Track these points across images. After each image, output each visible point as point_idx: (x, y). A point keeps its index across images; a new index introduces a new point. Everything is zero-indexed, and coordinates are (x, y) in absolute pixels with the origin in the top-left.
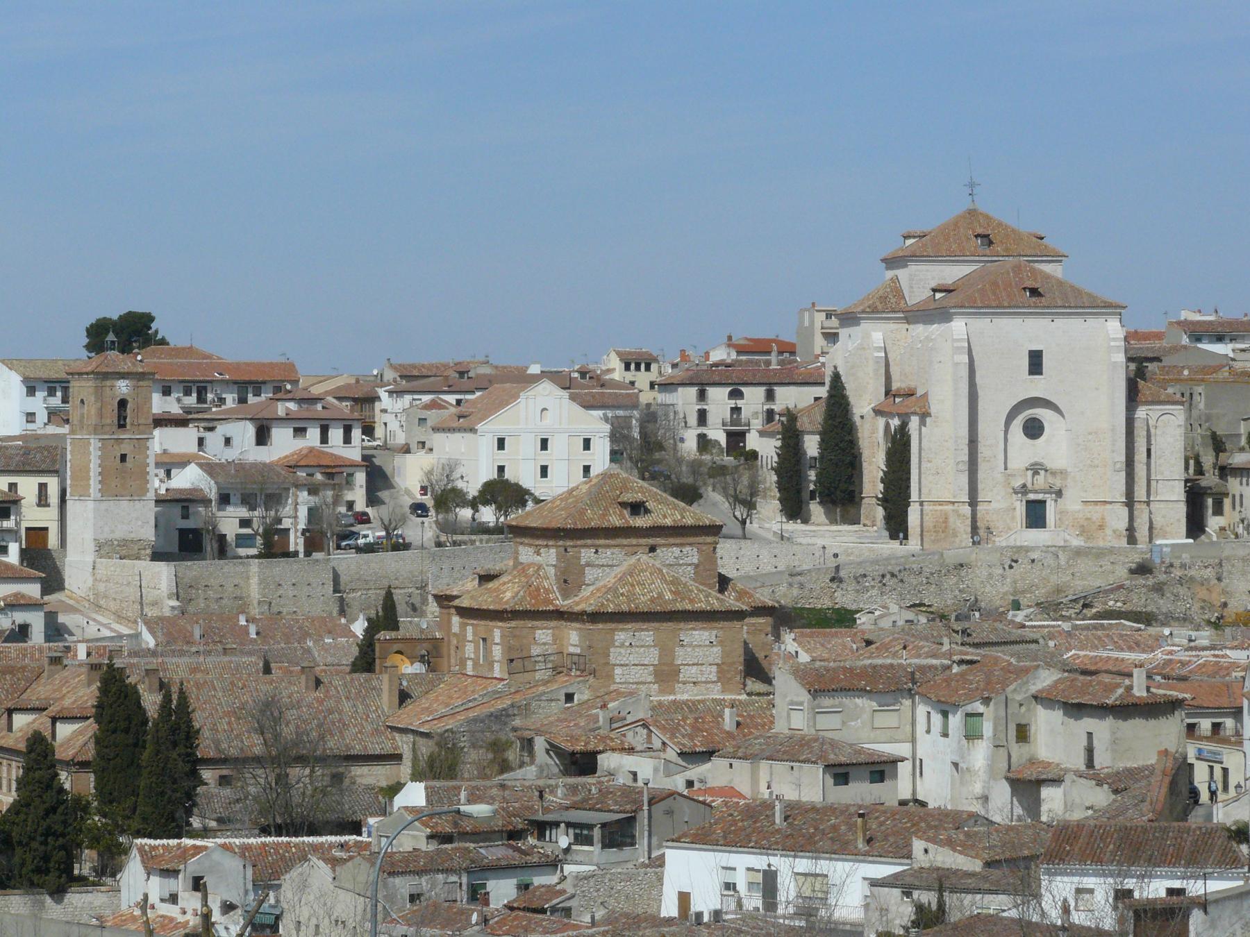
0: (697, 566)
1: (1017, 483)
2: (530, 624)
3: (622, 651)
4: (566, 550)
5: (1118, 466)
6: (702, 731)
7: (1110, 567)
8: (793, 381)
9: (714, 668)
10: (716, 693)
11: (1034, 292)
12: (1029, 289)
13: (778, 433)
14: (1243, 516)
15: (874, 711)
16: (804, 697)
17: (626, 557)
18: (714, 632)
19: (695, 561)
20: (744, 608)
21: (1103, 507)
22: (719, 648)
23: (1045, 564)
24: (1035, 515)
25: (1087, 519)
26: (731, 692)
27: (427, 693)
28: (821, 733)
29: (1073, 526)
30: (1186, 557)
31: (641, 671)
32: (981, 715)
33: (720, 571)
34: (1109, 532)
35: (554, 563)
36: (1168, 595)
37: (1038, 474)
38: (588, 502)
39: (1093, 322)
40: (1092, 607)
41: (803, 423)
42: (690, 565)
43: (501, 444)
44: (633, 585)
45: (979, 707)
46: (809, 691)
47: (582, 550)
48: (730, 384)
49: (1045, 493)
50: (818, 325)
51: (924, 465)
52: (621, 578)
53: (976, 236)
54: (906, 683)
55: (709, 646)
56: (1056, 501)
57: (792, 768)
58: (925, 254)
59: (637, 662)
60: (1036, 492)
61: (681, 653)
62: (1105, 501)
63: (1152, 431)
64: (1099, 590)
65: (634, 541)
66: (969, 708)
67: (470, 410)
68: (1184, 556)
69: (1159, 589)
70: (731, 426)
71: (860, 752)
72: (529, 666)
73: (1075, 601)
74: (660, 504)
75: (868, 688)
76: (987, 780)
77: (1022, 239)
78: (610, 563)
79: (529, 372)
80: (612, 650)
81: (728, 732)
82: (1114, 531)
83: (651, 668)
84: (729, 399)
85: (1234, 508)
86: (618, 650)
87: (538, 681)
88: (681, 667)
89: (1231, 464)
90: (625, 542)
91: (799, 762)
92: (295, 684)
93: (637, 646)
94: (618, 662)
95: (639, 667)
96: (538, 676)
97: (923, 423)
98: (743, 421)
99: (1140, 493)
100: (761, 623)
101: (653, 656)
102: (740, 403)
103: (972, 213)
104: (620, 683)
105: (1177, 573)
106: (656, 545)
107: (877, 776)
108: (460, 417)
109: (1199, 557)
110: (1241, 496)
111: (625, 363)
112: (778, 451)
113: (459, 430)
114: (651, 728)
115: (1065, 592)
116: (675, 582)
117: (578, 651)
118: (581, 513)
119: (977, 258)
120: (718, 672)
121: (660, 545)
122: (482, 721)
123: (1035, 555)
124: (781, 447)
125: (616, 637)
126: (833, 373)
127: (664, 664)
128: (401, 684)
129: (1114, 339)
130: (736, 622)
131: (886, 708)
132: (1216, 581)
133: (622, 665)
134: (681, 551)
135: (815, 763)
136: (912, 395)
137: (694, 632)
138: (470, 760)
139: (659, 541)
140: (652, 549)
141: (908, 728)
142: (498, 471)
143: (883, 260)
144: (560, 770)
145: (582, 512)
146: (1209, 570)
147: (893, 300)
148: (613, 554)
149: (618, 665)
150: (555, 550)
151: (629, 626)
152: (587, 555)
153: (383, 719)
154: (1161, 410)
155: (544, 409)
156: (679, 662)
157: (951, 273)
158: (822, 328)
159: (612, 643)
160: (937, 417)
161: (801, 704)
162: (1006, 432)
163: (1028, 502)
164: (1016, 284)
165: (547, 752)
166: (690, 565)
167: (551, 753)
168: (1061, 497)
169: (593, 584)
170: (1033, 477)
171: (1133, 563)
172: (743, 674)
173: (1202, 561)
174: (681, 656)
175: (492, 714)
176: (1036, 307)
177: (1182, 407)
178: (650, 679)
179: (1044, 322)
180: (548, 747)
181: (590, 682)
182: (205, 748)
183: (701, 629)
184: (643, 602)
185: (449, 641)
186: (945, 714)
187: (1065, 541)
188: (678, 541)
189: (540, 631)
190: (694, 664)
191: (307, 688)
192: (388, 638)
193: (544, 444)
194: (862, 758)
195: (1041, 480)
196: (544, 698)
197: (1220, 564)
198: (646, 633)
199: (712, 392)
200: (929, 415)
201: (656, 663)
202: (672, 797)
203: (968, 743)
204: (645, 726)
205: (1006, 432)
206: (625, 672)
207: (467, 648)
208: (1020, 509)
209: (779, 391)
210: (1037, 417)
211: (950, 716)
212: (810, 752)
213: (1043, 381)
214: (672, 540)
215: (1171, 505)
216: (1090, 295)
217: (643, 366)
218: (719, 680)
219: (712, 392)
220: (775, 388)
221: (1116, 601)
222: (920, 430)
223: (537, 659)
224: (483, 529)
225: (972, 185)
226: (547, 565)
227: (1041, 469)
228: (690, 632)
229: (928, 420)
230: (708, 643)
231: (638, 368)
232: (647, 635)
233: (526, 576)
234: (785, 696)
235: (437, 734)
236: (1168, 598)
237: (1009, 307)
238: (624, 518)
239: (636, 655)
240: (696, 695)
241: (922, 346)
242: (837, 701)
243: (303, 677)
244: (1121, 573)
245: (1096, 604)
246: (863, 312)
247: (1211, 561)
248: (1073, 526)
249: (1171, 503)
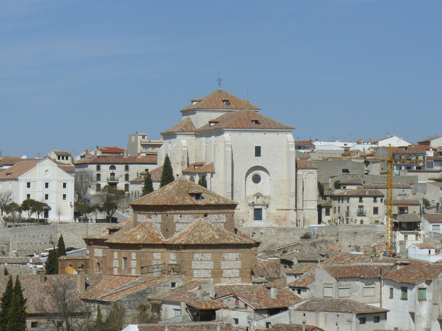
0: (225, 223)
1: (250, 202)
2: (151, 250)
3: (197, 262)
4: (167, 215)
5: (292, 194)
6: (262, 299)
7: (293, 236)
8: (137, 162)
9: (238, 271)
10: (238, 282)
11: (257, 122)
12: (255, 121)
13: (143, 182)
14: (340, 215)
15: (364, 288)
16: (334, 281)
17: (194, 219)
18: (238, 254)
19: (225, 221)
20: (252, 242)
21: (285, 211)
22: (240, 261)
23: (266, 235)
24: (258, 215)
25: (279, 216)
26: (245, 282)
27: (97, 283)
28: (341, 298)
29: (273, 219)
31: (206, 272)
32: (425, 289)
33: (235, 227)
34: (288, 222)
35: (160, 222)
36: (318, 247)
37: (259, 198)
38: (175, 193)
39: (281, 135)
40: (286, 252)
41: (153, 177)
42: (222, 223)
43: (29, 185)
44: (200, 232)
45: (424, 285)
46: (336, 278)
47: (175, 216)
48: (110, 163)
49: (262, 206)
50: (139, 141)
52: (194, 228)
53: (223, 101)
54: (378, 274)
55: (236, 260)
56: (266, 209)
57: (338, 315)
58: (203, 108)
59: (204, 268)
60: (258, 205)
61: (223, 264)
62: (286, 209)
63: (304, 180)
64: (289, 245)
65: (197, 211)
66: (420, 286)
67: (12, 171)
68: (323, 231)
69: (314, 245)
70: (110, 181)
71: (368, 307)
72: (150, 270)
73: (279, 250)
74: (207, 194)
75: (362, 277)
76: (429, 320)
77: (242, 102)
78: (187, 222)
79: (21, 158)
80: (193, 262)
81: (273, 300)
82: (291, 221)
83: (210, 271)
84: (110, 170)
85: (335, 212)
86: (196, 262)
87: (154, 277)
88: (223, 270)
89: (333, 194)
90: (194, 212)
91: (342, 312)
92: (35, 279)
93: (204, 260)
94: (195, 268)
95: (205, 270)
96: (155, 275)
97: (212, 176)
98: (115, 178)
100: (254, 250)
101: (211, 265)
102: (114, 171)
103: (220, 92)
104: (196, 278)
105: (320, 238)
106: (207, 214)
107: (376, 319)
108: (7, 174)
109: (329, 232)
110: (339, 207)
111: (58, 156)
112: (143, 189)
113: (8, 180)
114: (238, 297)
115: (275, 246)
116: (218, 230)
117: (175, 263)
118: (173, 198)
119: (224, 110)
120: (240, 273)
121: (209, 213)
122: (134, 296)
124: (144, 187)
125: (195, 256)
126: (166, 157)
127: (216, 269)
128: (86, 279)
129: (291, 142)
130: (247, 249)
131: (368, 286)
132: (336, 242)
133: (197, 269)
134: (218, 216)
135: (351, 313)
136: (202, 165)
137: (229, 254)
138: (128, 315)
139: (209, 211)
140: (206, 215)
141: (379, 296)
142: (27, 197)
143: (181, 111)
144: (192, 319)
145: (173, 198)
146: (333, 237)
147: (189, 127)
148: (188, 217)
149: (195, 269)
150: (161, 216)
151: (201, 251)
152: (176, 218)
153: (79, 295)
154: (308, 171)
155: (47, 171)
156: (223, 268)
157: (215, 116)
158: (141, 142)
159: (193, 259)
160: (217, 174)
161: (332, 284)
162: (246, 180)
163: (255, 209)
164: (248, 119)
165: (186, 309)
166: (222, 223)
167: (188, 310)
168: (268, 207)
169: (180, 231)
170: (257, 198)
171: (302, 234)
172: (251, 273)
173: (330, 234)
174: (223, 265)
175: (138, 293)
176: (259, 128)
177: (316, 170)
178: (210, 276)
179: (261, 135)
180: (187, 307)
181: (183, 277)
182: (30, 309)
183: (233, 252)
184: (206, 239)
185: (93, 261)
186: (404, 290)
187: (271, 225)
188: (217, 211)
189: (156, 254)
190: (229, 269)
191: (41, 281)
192: (65, 259)
193: (47, 185)
194: (371, 311)
195: (260, 201)
196: (162, 285)
197: (338, 235)
198: (208, 254)
199: (102, 167)
200: (214, 173)
201: (212, 268)
202: (315, 330)
203: (420, 302)
204: (235, 297)
205: (246, 180)
206: (199, 273)
207: (114, 262)
208: (252, 212)
209: (130, 166)
210: (258, 174)
211: (409, 291)
212: (346, 308)
213: (261, 159)
214: (214, 211)
215: (312, 211)
216: (279, 124)
217: (65, 158)
218: (240, 276)
219: (102, 167)
220: (129, 165)
221: (297, 250)
222: (211, 179)
223: (155, 266)
224: (24, 221)
225: (220, 80)
226: (155, 223)
227: (260, 196)
228: (228, 254)
229: (214, 175)
230: (235, 259)
231: (63, 159)
232: (208, 255)
233: (145, 228)
234: (321, 281)
235: (113, 302)
236: (317, 249)
237: (248, 128)
238: (193, 200)
239: (204, 265)
240: (231, 283)
241: (208, 145)
242: (348, 283)
243: (39, 276)
244: (298, 238)
245: (288, 251)
246: (178, 131)
248: (273, 219)
249: (312, 210)
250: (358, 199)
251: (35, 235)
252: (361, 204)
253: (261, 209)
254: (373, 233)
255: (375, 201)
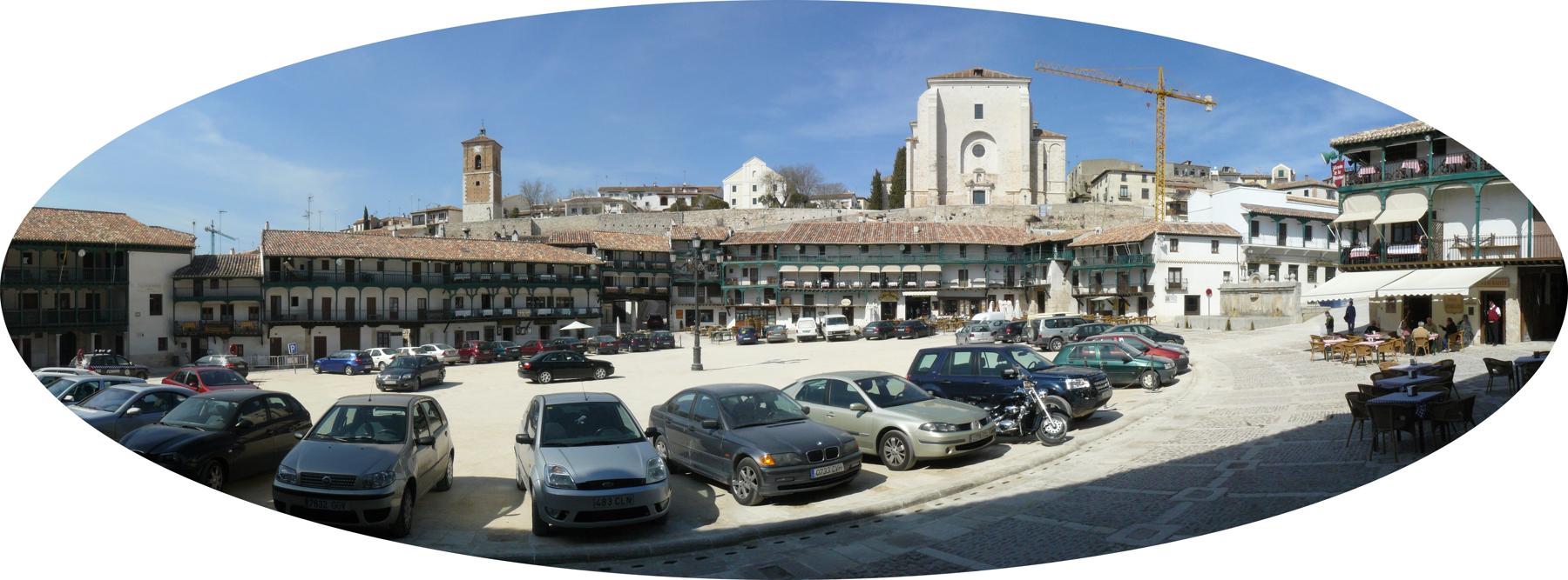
1: (968, 180)
24: (979, 197)
30: (1062, 213)
51: (915, 171)
60: (979, 185)
97: (914, 146)
99: (1040, 188)
123: (965, 211)
146: (1077, 220)
155: (754, 172)
197: (1083, 217)
208: (970, 195)
247: (1077, 215)
250: (1120, 176)
251: (643, 224)
252: (1124, 183)
253: (984, 192)
254: (1139, 217)
255: (1144, 181)
